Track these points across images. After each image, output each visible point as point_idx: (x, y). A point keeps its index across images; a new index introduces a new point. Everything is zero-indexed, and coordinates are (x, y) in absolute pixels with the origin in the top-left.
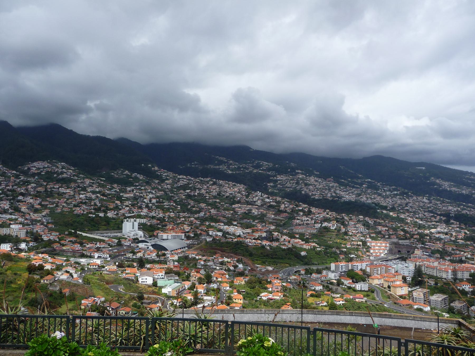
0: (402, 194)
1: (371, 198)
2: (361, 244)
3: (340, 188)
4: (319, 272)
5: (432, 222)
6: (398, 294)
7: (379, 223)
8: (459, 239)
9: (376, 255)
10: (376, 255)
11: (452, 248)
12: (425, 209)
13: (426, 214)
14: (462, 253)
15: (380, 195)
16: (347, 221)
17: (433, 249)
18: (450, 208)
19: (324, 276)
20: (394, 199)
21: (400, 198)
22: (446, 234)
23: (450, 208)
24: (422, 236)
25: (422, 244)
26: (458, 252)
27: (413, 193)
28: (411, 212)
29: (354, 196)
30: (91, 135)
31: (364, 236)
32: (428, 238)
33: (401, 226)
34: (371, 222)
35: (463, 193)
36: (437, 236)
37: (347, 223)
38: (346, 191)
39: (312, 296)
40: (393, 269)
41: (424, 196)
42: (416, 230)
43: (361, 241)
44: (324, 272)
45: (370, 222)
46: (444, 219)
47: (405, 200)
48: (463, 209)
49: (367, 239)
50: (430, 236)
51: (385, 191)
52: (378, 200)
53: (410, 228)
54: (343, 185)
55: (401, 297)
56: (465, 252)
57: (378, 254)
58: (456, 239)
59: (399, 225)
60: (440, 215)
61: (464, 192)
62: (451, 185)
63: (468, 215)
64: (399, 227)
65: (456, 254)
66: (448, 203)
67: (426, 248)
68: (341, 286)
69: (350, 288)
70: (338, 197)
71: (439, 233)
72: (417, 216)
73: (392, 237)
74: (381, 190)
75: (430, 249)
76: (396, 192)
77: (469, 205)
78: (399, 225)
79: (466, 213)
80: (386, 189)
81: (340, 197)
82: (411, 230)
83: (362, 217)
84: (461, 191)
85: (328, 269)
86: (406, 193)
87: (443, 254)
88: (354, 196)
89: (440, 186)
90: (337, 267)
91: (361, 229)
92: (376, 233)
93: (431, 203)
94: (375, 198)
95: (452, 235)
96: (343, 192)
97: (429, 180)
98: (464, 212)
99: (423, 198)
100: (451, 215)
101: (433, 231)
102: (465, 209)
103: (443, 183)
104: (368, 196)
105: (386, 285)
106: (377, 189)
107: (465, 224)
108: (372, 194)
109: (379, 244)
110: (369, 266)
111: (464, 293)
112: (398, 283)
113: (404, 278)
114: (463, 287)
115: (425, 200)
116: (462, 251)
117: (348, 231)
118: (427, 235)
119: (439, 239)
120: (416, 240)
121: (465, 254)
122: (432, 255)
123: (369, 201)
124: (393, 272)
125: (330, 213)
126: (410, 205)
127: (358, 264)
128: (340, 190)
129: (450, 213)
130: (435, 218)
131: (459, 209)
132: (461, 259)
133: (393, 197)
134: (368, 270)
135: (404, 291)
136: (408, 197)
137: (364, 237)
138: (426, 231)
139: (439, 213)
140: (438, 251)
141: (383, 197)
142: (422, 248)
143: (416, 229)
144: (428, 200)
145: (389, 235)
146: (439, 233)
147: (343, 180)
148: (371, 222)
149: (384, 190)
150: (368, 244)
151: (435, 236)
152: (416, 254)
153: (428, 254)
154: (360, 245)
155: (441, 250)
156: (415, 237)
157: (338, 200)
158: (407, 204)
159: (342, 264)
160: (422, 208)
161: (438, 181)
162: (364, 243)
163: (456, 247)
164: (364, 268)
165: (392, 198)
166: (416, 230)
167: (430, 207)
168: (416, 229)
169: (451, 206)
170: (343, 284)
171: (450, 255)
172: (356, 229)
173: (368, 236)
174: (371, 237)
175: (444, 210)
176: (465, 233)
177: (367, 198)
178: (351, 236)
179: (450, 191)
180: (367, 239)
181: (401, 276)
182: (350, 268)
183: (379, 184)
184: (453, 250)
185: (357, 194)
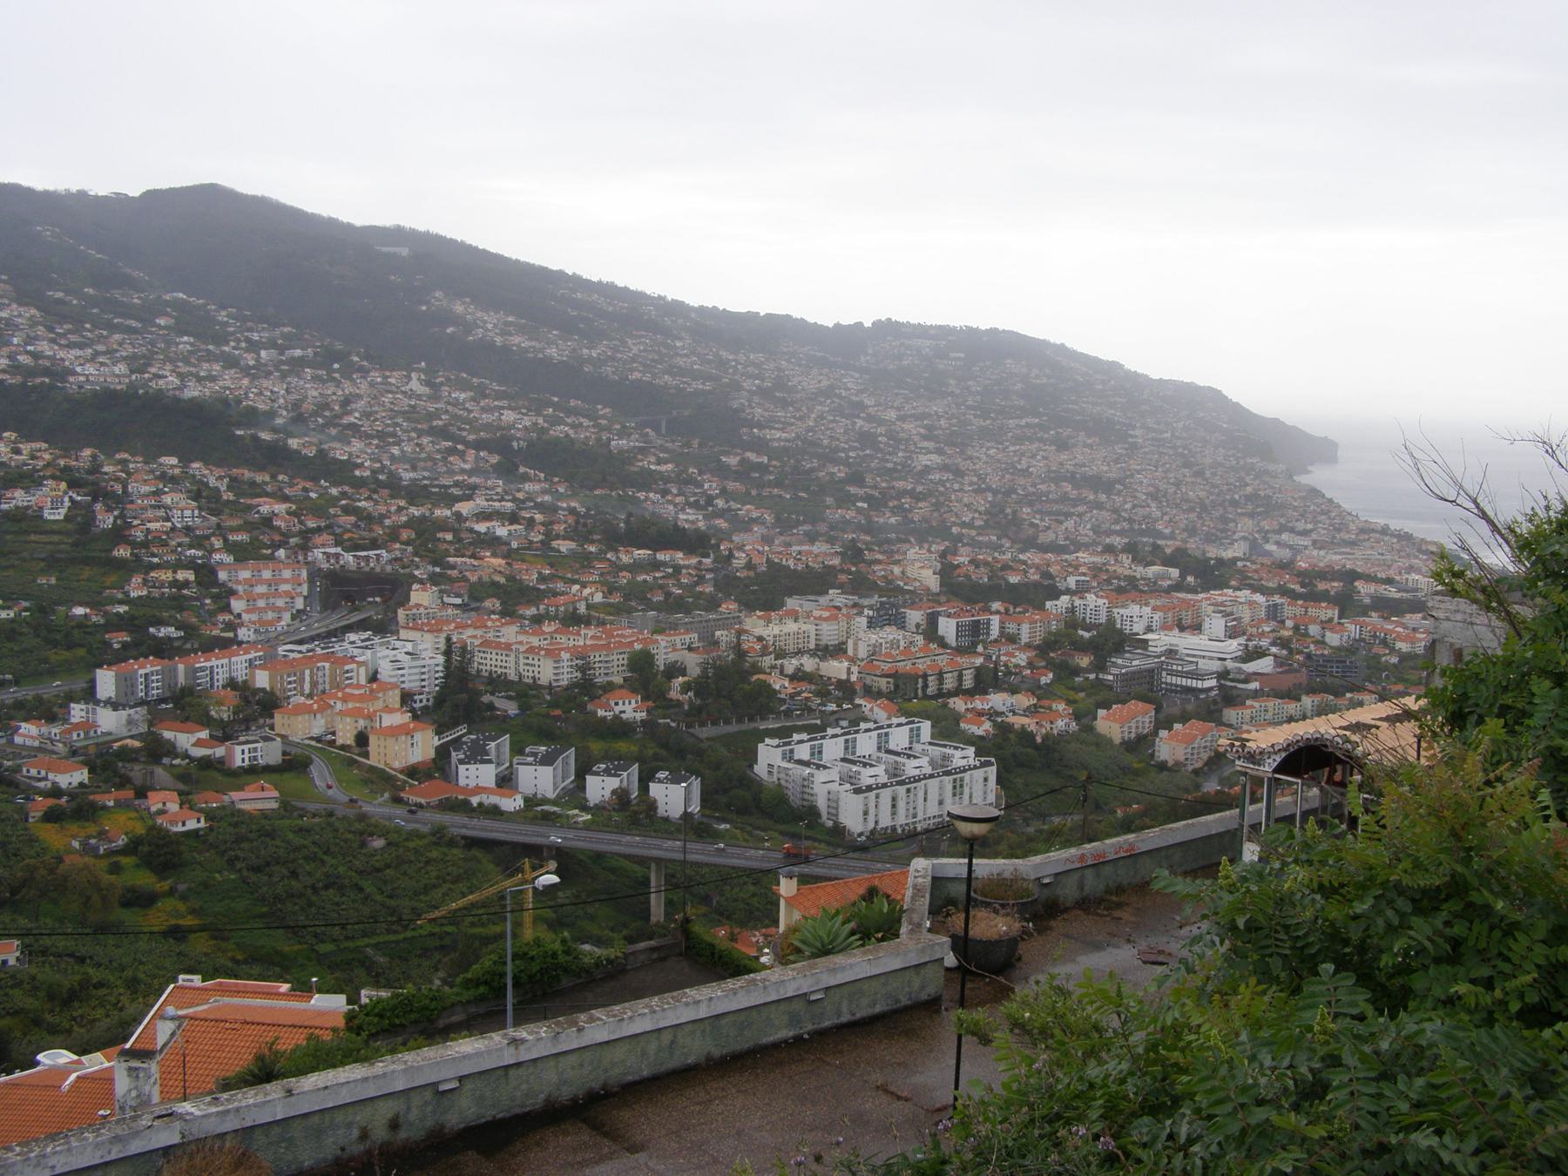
0: (326, 359)
1: (199, 379)
2: (192, 577)
3: (51, 330)
4: (49, 712)
5: (451, 472)
6: (397, 765)
7: (253, 484)
8: (557, 537)
9: (261, 622)
10: (261, 622)
11: (540, 573)
12: (417, 421)
13: (425, 440)
14: (577, 587)
15: (231, 362)
16: (117, 479)
17: (474, 578)
18: (509, 416)
19: (77, 726)
20: (293, 380)
21: (315, 378)
22: (513, 518)
23: (509, 416)
24: (425, 531)
25: (435, 564)
26: (560, 586)
27: (368, 357)
28: (369, 437)
29: (121, 368)
30: (1127, 366)
31: (199, 542)
32: (449, 537)
33: (344, 495)
34: (214, 478)
35: (552, 358)
36: (481, 527)
37: (119, 489)
38: (81, 346)
39: (52, 816)
40: (362, 670)
41: (410, 370)
42: (400, 509)
43: (191, 565)
44: (77, 712)
45: (212, 482)
46: (495, 459)
47: (338, 384)
48: (556, 421)
49: (217, 557)
50: (455, 532)
51: (254, 347)
52: (228, 383)
53: (376, 502)
54: (63, 318)
55: (412, 771)
56: (584, 586)
57: (270, 615)
58: (549, 536)
59: (334, 491)
60: (479, 445)
61: (552, 352)
62: (507, 324)
63: (572, 441)
64: (333, 501)
65: (555, 594)
66: (499, 396)
67: (451, 580)
68: (166, 760)
69: (206, 764)
70: (47, 372)
71: (483, 516)
72: (396, 451)
73: (318, 540)
74: (238, 341)
75: (465, 579)
76: (298, 352)
77: (573, 403)
78: (334, 491)
79: (567, 435)
80: (256, 337)
81: (60, 373)
82: (382, 509)
83: (174, 461)
84: (542, 350)
85: (89, 695)
86: (341, 357)
87: (513, 598)
88: (121, 368)
89: (469, 328)
90: (126, 683)
91: (188, 513)
92: (248, 527)
93: (435, 398)
94: (213, 379)
95: (532, 520)
96: (70, 346)
97: (427, 303)
98: (560, 431)
99: (409, 378)
100: (515, 444)
101: (465, 508)
102: (560, 422)
103: (479, 314)
104: (184, 369)
105: (346, 736)
106: (221, 339)
107: (569, 479)
108: (200, 360)
109: (267, 574)
110: (261, 667)
111: (620, 729)
112: (390, 720)
113: (407, 698)
114: (617, 709)
115: (415, 385)
116: (575, 582)
117: (130, 526)
118: (443, 526)
119: (492, 542)
120: (410, 549)
121: (587, 591)
122: (474, 605)
123: (192, 391)
124: (363, 681)
125: (26, 448)
126: (361, 404)
127: (214, 662)
128: (53, 341)
129: (514, 438)
130: (462, 455)
131: (540, 421)
132: (575, 609)
133: (290, 372)
134: (262, 680)
135: (422, 746)
136: (349, 371)
137: (199, 546)
138: (438, 512)
139: (472, 437)
140: (494, 589)
141: (246, 370)
142: (434, 579)
143: (402, 503)
144: (428, 383)
145: (306, 534)
146: (483, 516)
147: (60, 295)
148: (214, 478)
149: (248, 340)
150: (222, 576)
151: (471, 531)
152: (418, 606)
153: (458, 601)
154: (186, 584)
155: (502, 580)
156: (405, 535)
157: (51, 387)
158: (346, 402)
159: (148, 669)
160: (408, 420)
161: (459, 308)
162: (206, 573)
163: (552, 565)
164: (241, 674)
165: (284, 376)
166: (400, 509)
167: (436, 415)
168: (402, 503)
169: (510, 408)
170: (171, 750)
171: (531, 595)
172: (161, 513)
173: (218, 543)
174: (230, 547)
175: (488, 427)
176: (572, 511)
177: (181, 376)
178: (145, 544)
179: (506, 349)
180: (217, 557)
181: (397, 692)
182: (181, 680)
183: (222, 316)
184: (542, 579)
185: (134, 357)
